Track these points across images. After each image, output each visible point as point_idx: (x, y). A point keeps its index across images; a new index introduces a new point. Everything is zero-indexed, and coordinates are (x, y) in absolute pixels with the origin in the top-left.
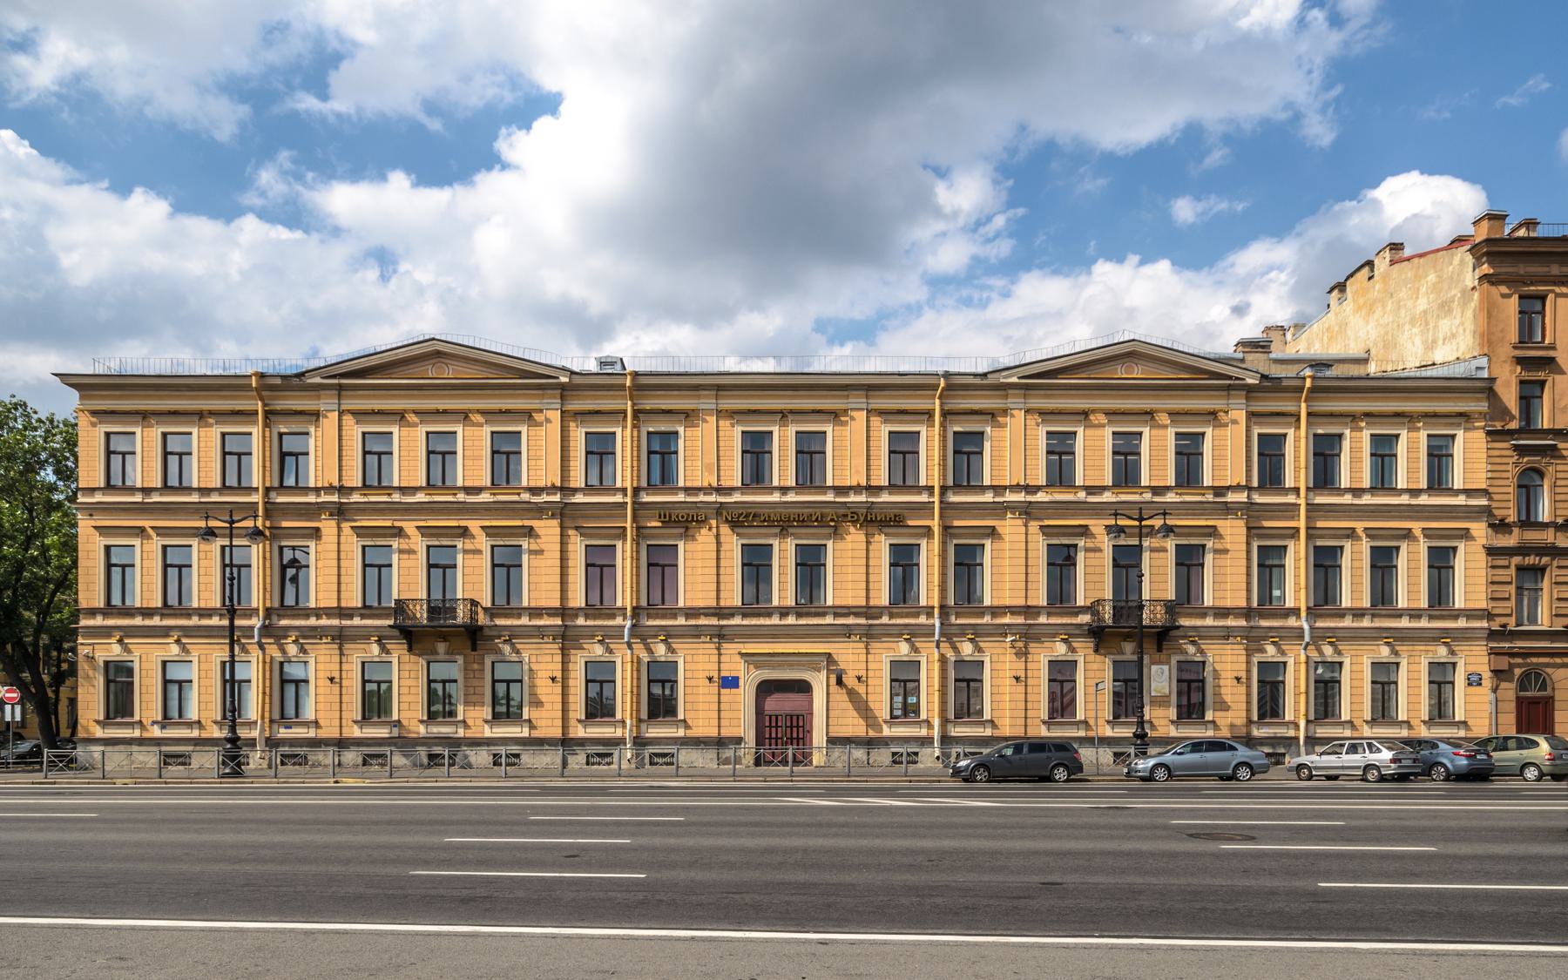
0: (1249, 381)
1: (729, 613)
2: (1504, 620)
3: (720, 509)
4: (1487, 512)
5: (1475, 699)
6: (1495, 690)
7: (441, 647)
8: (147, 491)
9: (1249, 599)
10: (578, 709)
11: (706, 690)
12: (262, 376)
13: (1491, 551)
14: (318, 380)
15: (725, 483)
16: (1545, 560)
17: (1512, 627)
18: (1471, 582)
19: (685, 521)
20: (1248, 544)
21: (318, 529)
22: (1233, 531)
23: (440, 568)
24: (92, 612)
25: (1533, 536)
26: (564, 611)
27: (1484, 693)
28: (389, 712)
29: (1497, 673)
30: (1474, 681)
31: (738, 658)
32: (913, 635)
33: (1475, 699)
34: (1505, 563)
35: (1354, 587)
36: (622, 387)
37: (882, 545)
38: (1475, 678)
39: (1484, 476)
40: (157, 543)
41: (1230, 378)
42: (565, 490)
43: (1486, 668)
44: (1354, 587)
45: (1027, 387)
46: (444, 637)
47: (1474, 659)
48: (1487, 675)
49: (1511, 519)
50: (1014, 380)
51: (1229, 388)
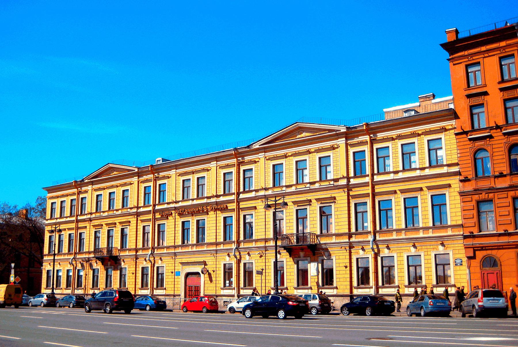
0: (342, 131)
1: (220, 244)
2: (471, 229)
3: (175, 209)
4: (459, 173)
5: (459, 272)
6: (469, 267)
7: (302, 254)
8: (396, 172)
9: (349, 229)
10: (139, 285)
11: (344, 272)
12: (152, 166)
13: (462, 194)
14: (87, 181)
15: (178, 200)
16: (491, 195)
17: (511, 231)
18: (454, 211)
19: (166, 214)
20: (349, 203)
21: (335, 198)
22: (341, 196)
23: (301, 219)
24: (46, 255)
25: (484, 184)
26: (137, 250)
27: (464, 271)
28: (394, 282)
29: (469, 258)
30: (458, 264)
31: (180, 265)
32: (442, 241)
33: (459, 272)
34: (469, 199)
35: (398, 219)
36: (73, 186)
37: (221, 216)
38: (458, 261)
39: (456, 156)
40: (401, 197)
41: (334, 131)
42: (138, 208)
43: (464, 255)
44: (398, 219)
45: (264, 148)
46: (302, 249)
47: (456, 251)
48: (465, 260)
49: (505, 173)
50: (258, 147)
51: (337, 135)
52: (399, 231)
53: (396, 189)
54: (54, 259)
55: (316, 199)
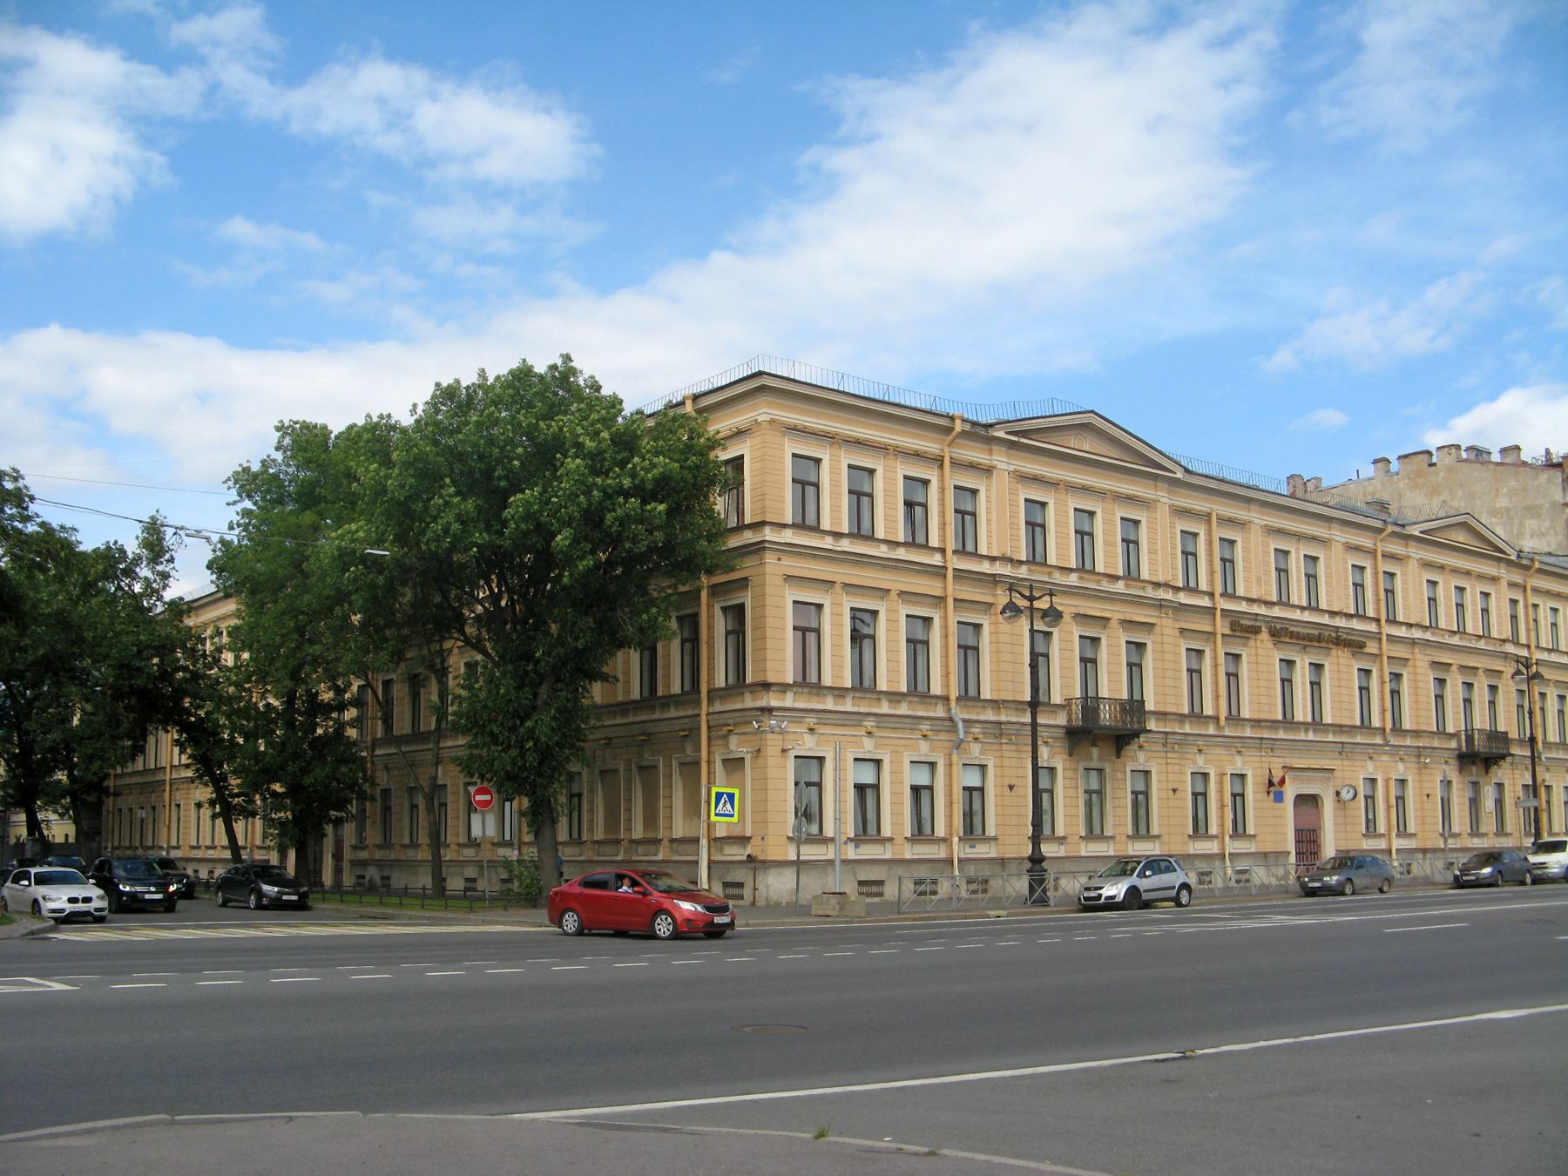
14: (1001, 434)
52: (839, 692)
53: (839, 579)
54: (1034, 724)
55: (902, 593)
